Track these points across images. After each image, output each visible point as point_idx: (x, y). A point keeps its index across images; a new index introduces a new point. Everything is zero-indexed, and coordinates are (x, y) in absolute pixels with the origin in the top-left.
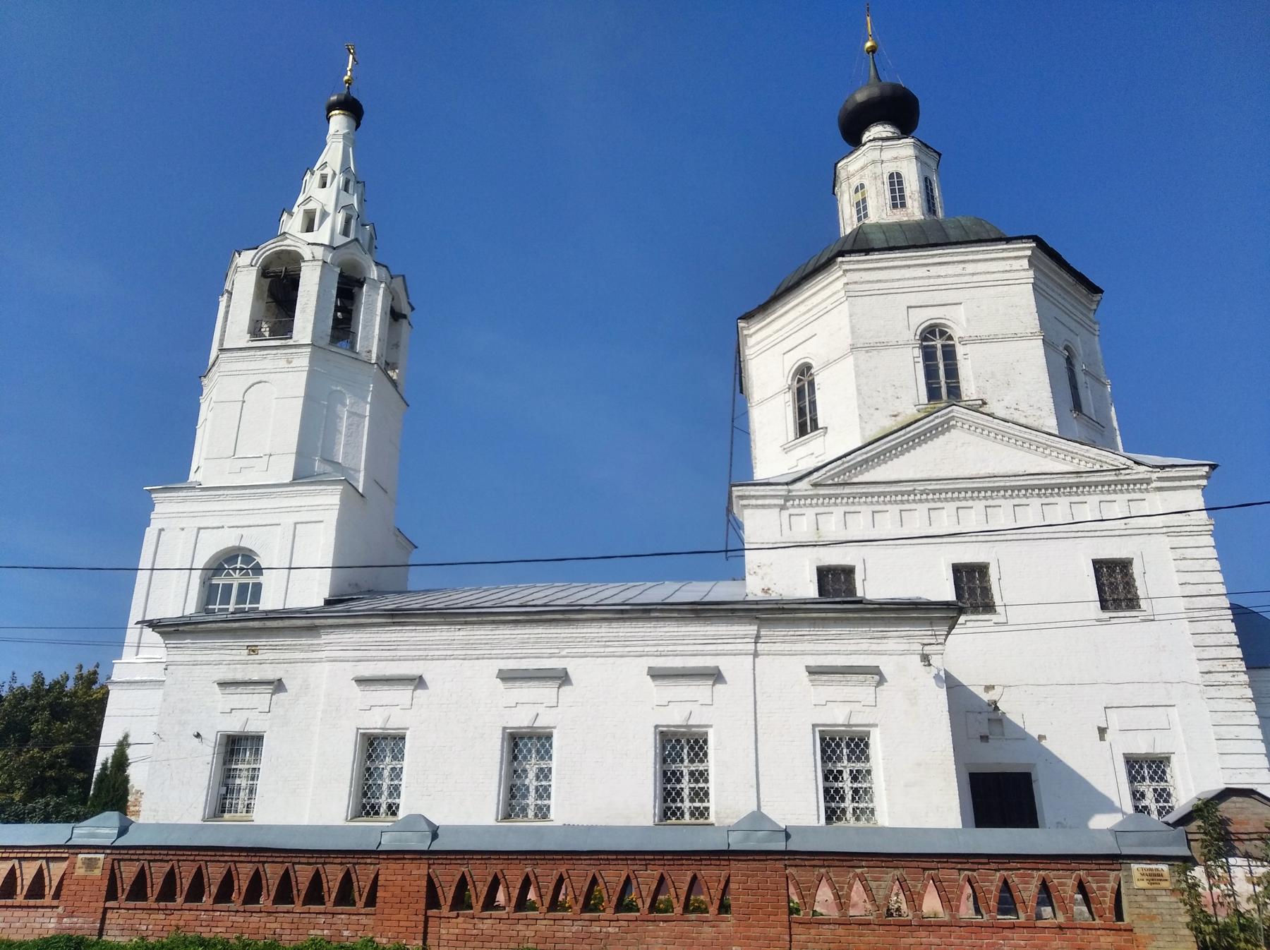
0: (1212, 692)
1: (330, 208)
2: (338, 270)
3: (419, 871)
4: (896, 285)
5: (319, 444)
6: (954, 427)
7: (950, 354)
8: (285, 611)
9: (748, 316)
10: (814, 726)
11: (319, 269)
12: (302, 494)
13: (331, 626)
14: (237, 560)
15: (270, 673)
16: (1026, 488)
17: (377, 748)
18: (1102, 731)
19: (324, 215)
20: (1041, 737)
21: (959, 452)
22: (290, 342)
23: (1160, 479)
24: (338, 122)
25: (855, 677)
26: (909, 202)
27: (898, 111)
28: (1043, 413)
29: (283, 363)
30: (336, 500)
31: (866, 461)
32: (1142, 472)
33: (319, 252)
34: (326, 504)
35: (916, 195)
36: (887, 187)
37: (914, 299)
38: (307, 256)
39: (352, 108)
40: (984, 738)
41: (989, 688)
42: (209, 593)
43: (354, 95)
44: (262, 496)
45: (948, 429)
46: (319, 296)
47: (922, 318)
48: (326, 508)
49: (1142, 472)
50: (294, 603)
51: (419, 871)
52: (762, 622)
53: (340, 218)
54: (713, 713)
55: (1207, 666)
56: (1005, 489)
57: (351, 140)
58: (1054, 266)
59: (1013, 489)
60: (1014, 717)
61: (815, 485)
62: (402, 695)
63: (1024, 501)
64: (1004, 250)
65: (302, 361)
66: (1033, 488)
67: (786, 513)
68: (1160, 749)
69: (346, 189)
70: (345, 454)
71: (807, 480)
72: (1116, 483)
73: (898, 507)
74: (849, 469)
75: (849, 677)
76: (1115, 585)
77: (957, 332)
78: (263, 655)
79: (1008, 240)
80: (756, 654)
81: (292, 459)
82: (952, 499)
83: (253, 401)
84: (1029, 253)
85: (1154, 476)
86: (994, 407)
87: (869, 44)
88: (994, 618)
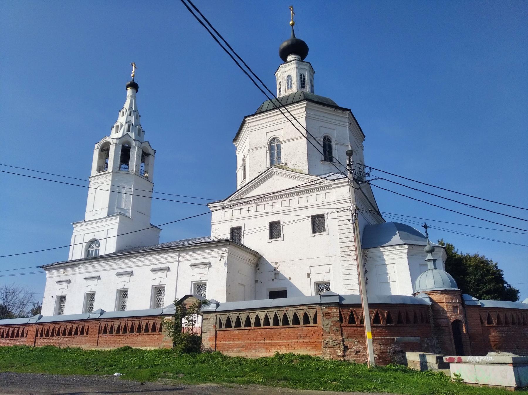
0: (343, 259)
1: (124, 124)
2: (121, 145)
3: (35, 328)
4: (263, 125)
5: (116, 203)
6: (274, 174)
7: (279, 146)
8: (105, 255)
9: (235, 140)
10: (192, 282)
11: (114, 147)
12: (110, 220)
13: (79, 264)
14: (94, 242)
15: (67, 278)
16: (293, 193)
17: (91, 297)
18: (309, 275)
19: (122, 125)
20: (290, 278)
21: (279, 182)
22: (107, 172)
23: (334, 184)
24: (130, 91)
25: (202, 266)
26: (293, 85)
27: (298, 49)
28: (304, 165)
29: (105, 179)
30: (118, 221)
31: (247, 190)
32: (328, 183)
33: (115, 141)
34: (115, 221)
35: (295, 83)
36: (286, 81)
37: (268, 130)
38: (112, 143)
39: (134, 86)
40: (273, 280)
41: (276, 263)
42: (88, 252)
43: (135, 81)
44: (100, 222)
45: (273, 175)
46: (115, 155)
47: (270, 136)
48: (115, 224)
49: (328, 183)
50: (108, 252)
51: (35, 328)
52: (180, 251)
53: (127, 126)
54: (166, 280)
55: (343, 249)
56: (286, 194)
57: (134, 97)
58: (321, 106)
59: (289, 194)
60: (282, 272)
61: (231, 201)
62: (94, 282)
63: (293, 198)
64: (297, 106)
65: (110, 177)
66: (295, 193)
67: (224, 211)
68: (326, 280)
69: (130, 115)
70: (125, 205)
71: (228, 200)
72: (321, 187)
73: (255, 205)
74: (242, 194)
75: (201, 266)
76: (318, 223)
77: (281, 139)
78: (67, 273)
79: (298, 102)
80: (179, 262)
81: (107, 209)
82: (271, 200)
83: (99, 192)
84: (305, 105)
85: (332, 183)
86: (290, 166)
87: (291, 22)
88: (280, 239)
